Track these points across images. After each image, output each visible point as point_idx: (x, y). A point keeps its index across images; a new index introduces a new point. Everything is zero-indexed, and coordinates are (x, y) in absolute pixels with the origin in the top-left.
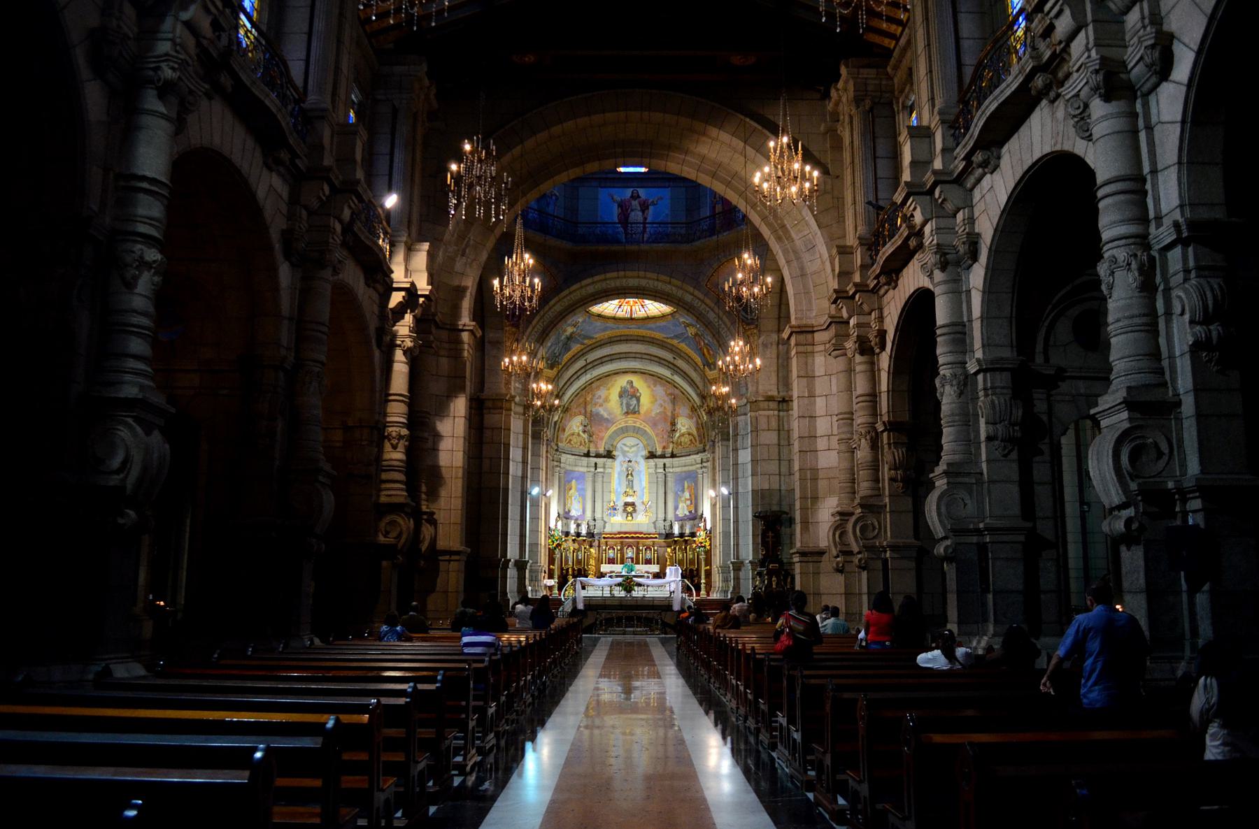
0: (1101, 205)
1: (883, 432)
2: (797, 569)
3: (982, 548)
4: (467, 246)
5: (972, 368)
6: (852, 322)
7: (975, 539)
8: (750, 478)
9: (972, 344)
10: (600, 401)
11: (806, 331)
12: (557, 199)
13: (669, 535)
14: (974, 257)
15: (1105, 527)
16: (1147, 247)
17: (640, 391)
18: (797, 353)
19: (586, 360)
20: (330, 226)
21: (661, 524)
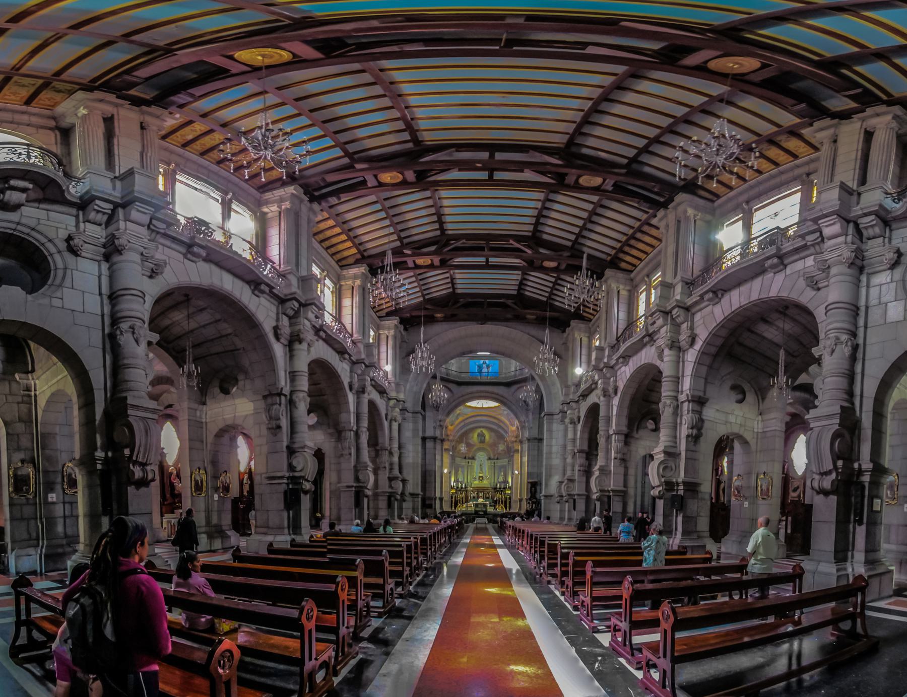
2: (543, 501)
3: (609, 497)
5: (611, 432)
6: (568, 412)
11: (550, 415)
13: (495, 488)
15: (652, 493)
16: (677, 400)
21: (492, 484)
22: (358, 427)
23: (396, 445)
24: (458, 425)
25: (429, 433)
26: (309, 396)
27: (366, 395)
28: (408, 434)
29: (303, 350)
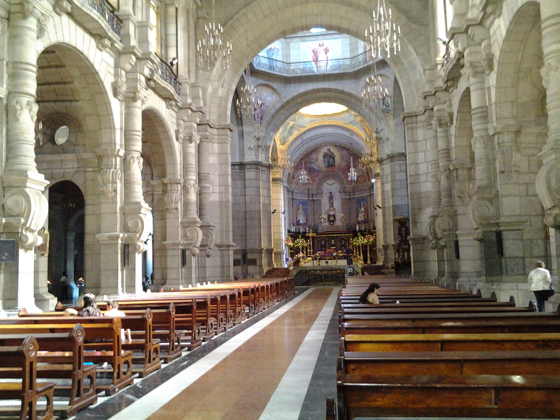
0: (544, 33)
1: (453, 170)
3: (499, 234)
4: (224, 82)
6: (435, 109)
7: (494, 229)
8: (391, 199)
9: (491, 118)
10: (313, 161)
12: (278, 50)
14: (491, 67)
17: (335, 154)
18: (407, 128)
19: (302, 139)
20: (137, 78)
22: (128, 150)
23: (193, 177)
24: (292, 143)
25: (250, 157)
26: (38, 102)
27: (138, 103)
28: (212, 160)
29: (192, 147)
